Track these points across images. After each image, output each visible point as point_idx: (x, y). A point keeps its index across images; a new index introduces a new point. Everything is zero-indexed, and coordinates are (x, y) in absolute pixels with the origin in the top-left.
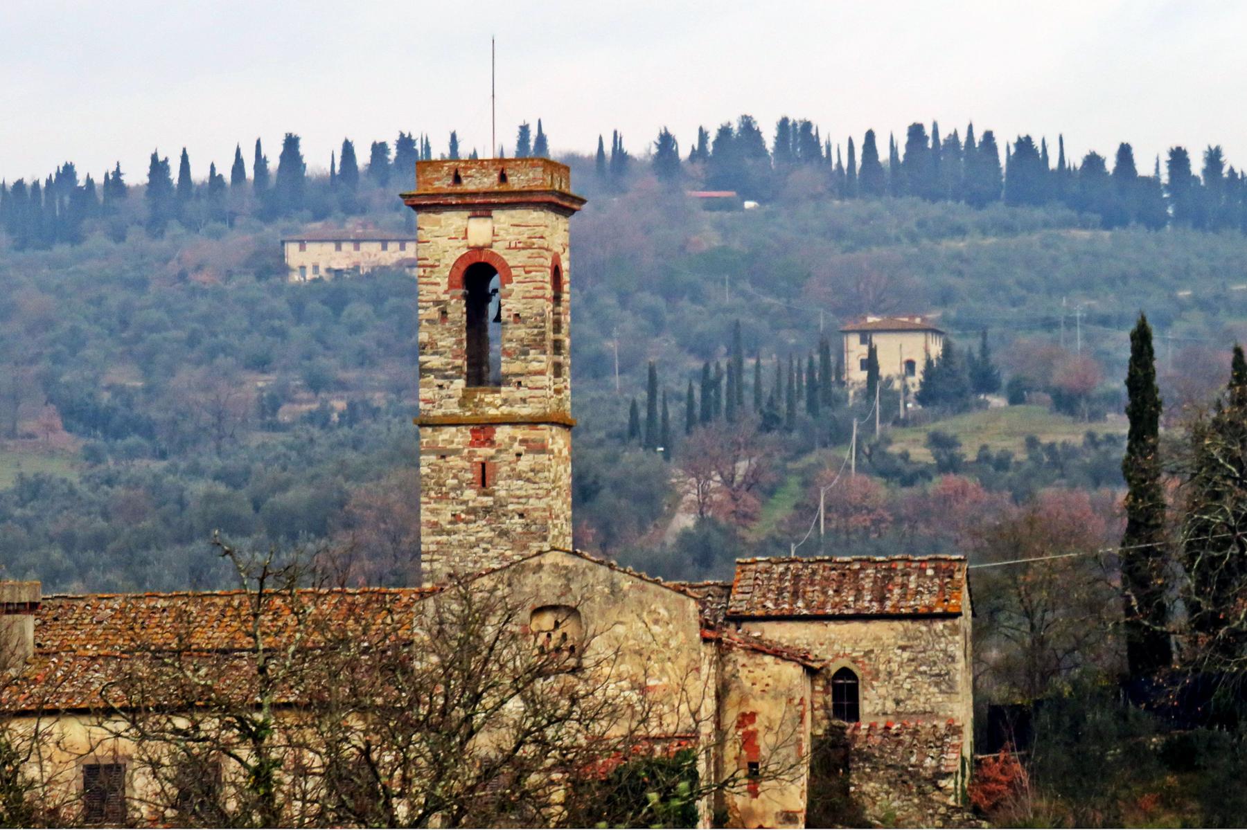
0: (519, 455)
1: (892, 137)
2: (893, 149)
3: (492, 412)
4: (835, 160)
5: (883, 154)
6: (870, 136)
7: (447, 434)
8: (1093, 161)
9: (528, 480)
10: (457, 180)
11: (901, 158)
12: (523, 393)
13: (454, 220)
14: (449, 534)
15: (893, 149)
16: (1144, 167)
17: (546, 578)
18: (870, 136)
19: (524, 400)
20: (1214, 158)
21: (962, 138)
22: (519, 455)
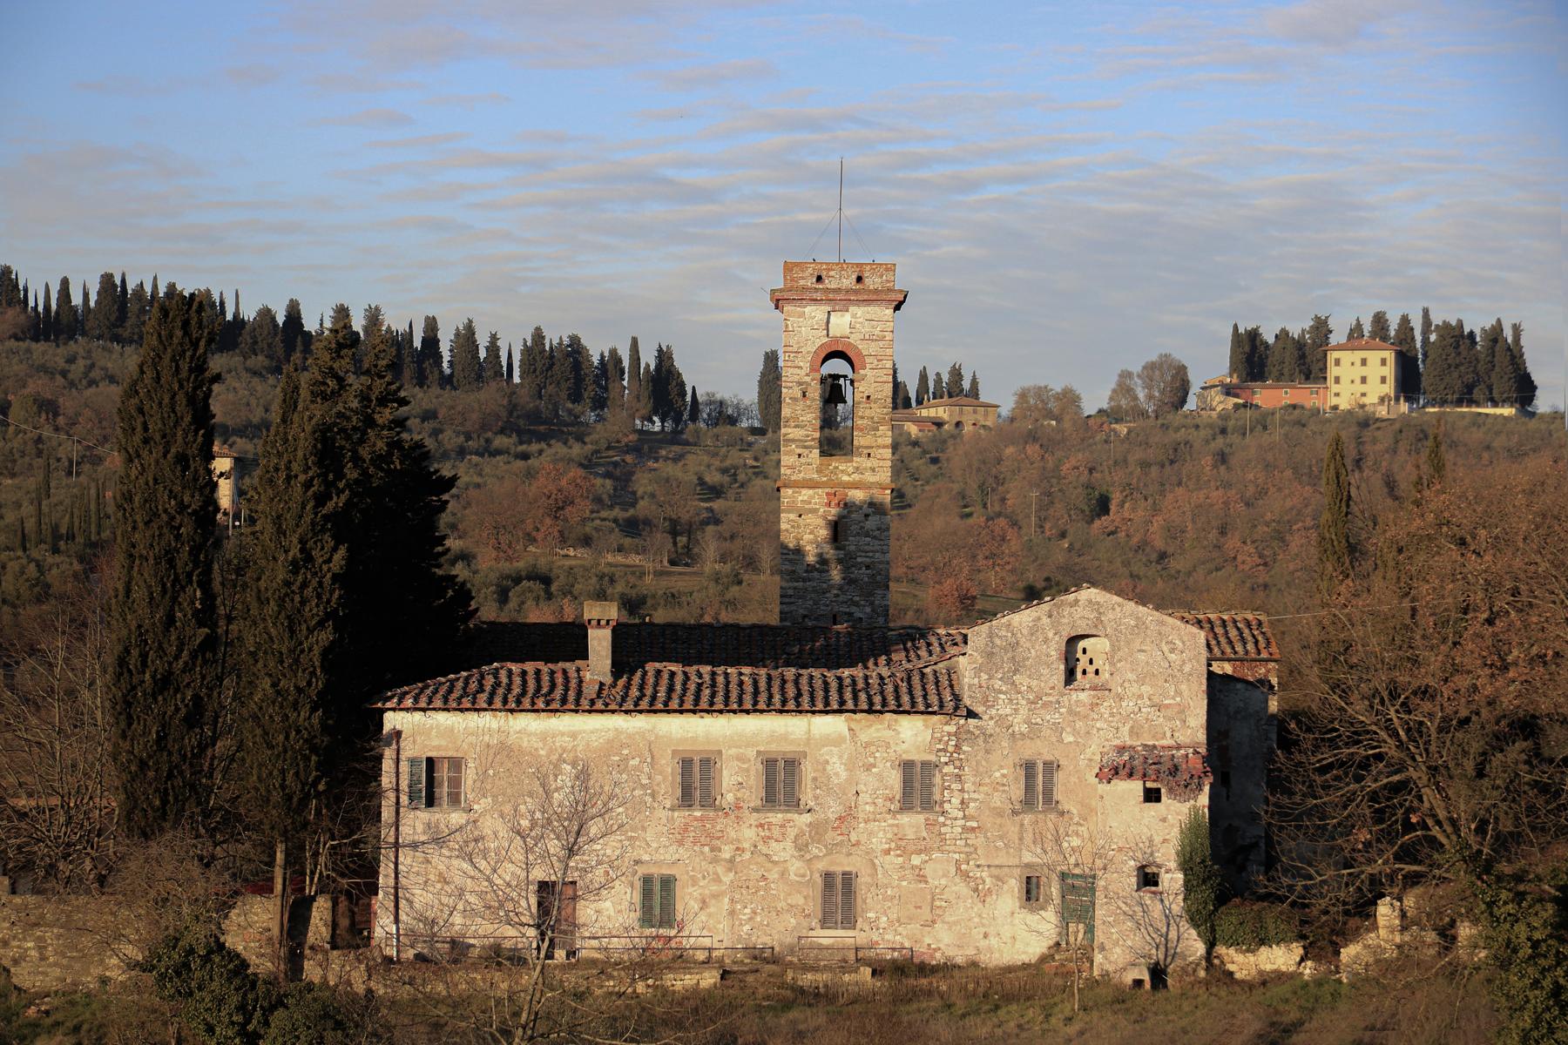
0: (867, 516)
1: (85, 288)
2: (86, 296)
3: (845, 478)
4: (31, 303)
5: (77, 300)
6: (65, 283)
7: (806, 494)
8: (266, 314)
9: (874, 537)
10: (819, 279)
11: (92, 304)
12: (868, 463)
13: (816, 313)
14: (804, 580)
15: (86, 296)
16: (310, 324)
17: (1079, 612)
18: (65, 283)
19: (873, 470)
20: (374, 317)
21: (148, 289)
22: (867, 516)
